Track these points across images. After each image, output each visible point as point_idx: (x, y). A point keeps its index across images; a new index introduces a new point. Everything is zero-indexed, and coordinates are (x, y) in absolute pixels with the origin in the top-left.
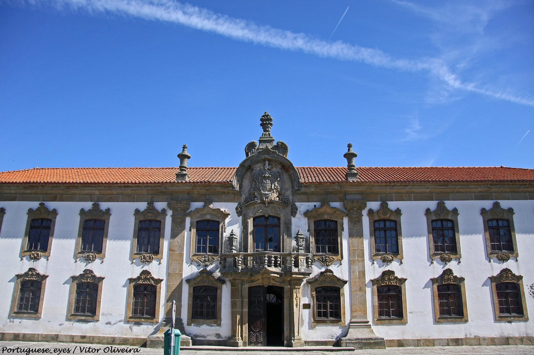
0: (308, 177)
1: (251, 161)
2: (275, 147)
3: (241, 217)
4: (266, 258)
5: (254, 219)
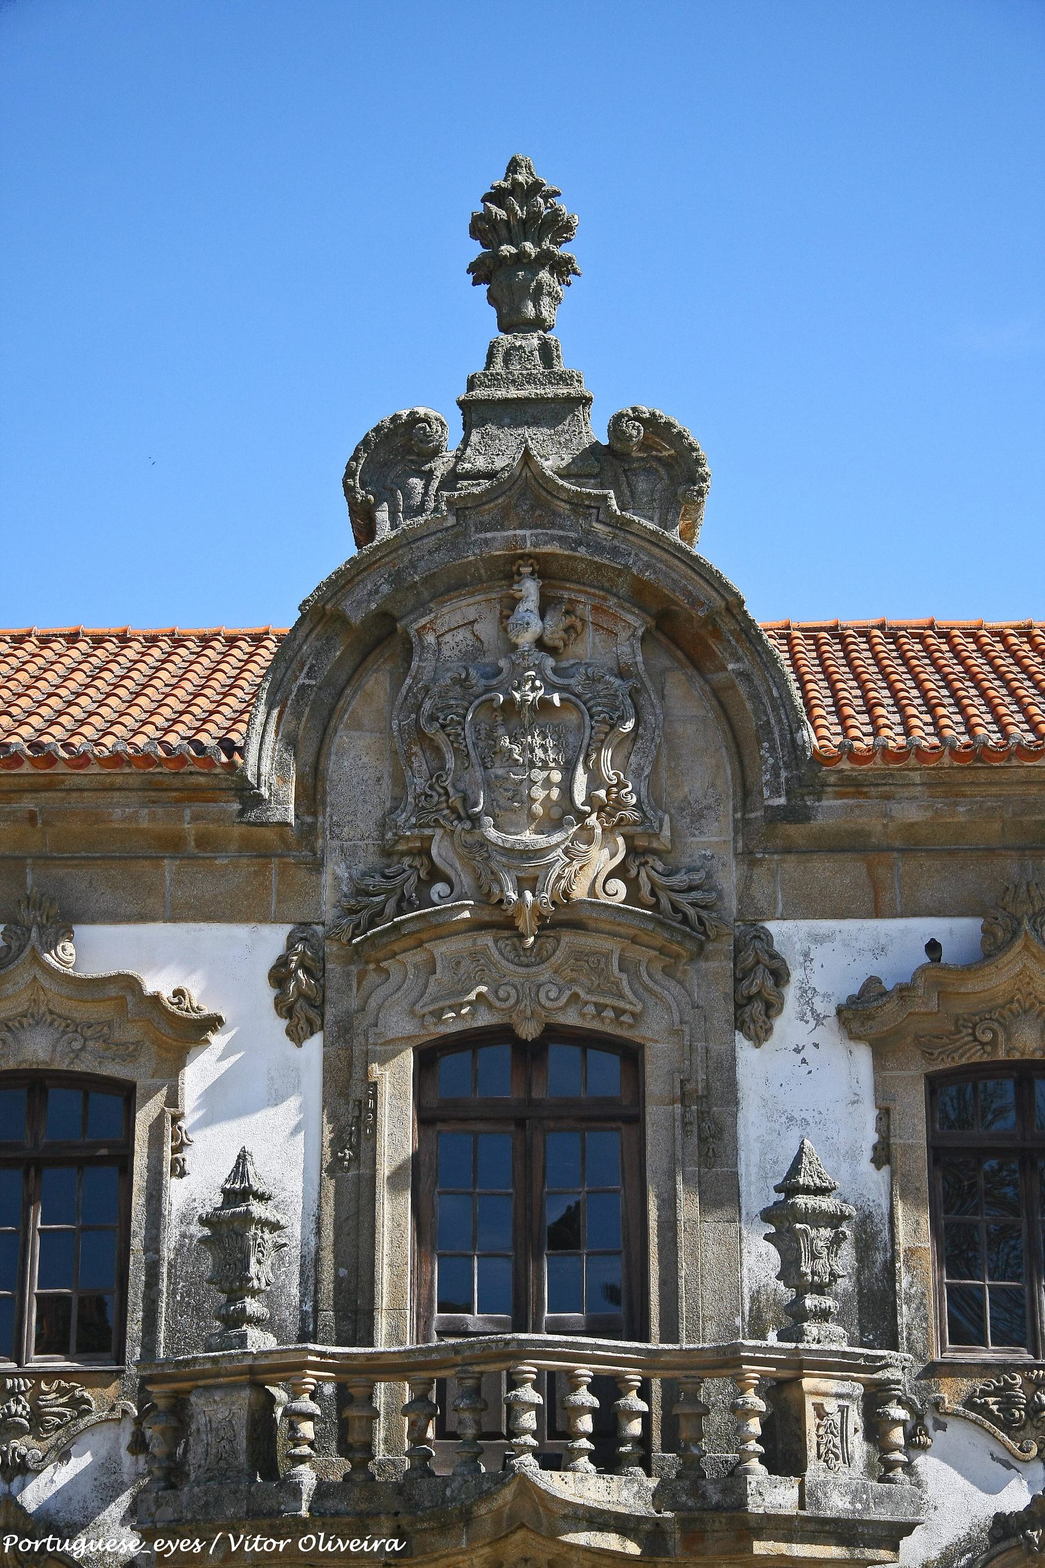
0: (869, 708)
1: (396, 579)
2: (606, 461)
3: (315, 1045)
4: (529, 1394)
5: (427, 1060)
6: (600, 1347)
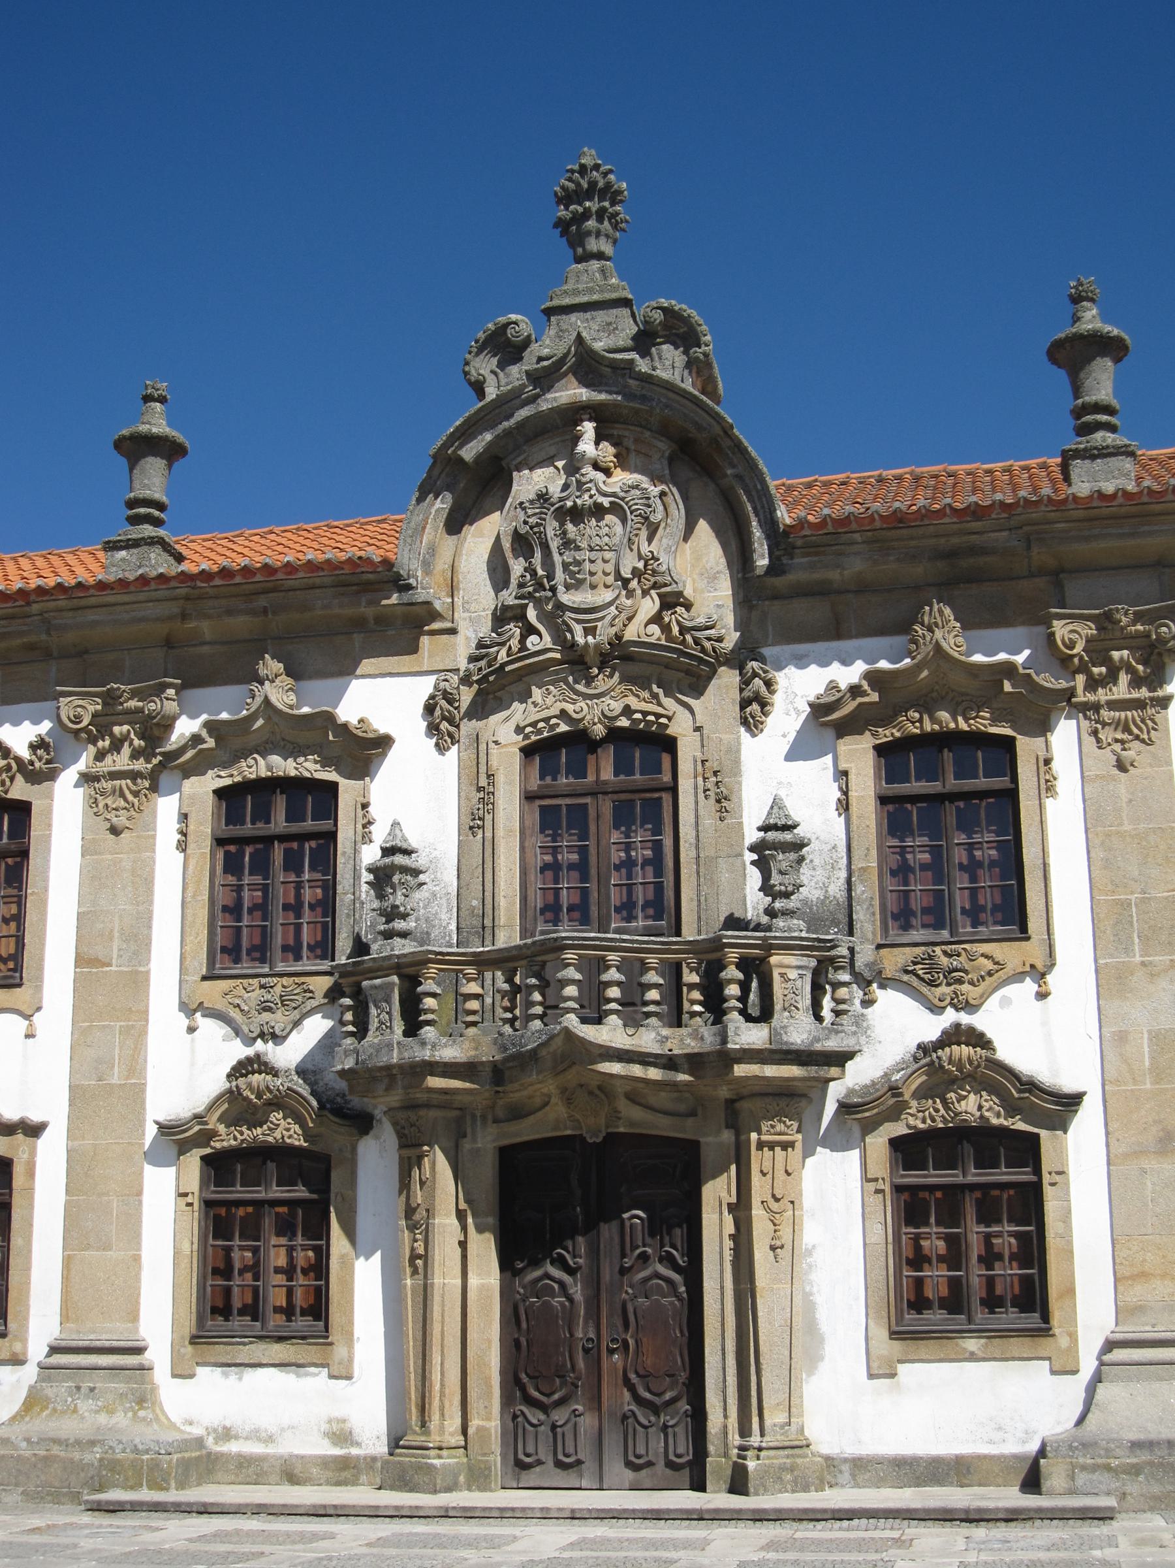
6: (624, 941)
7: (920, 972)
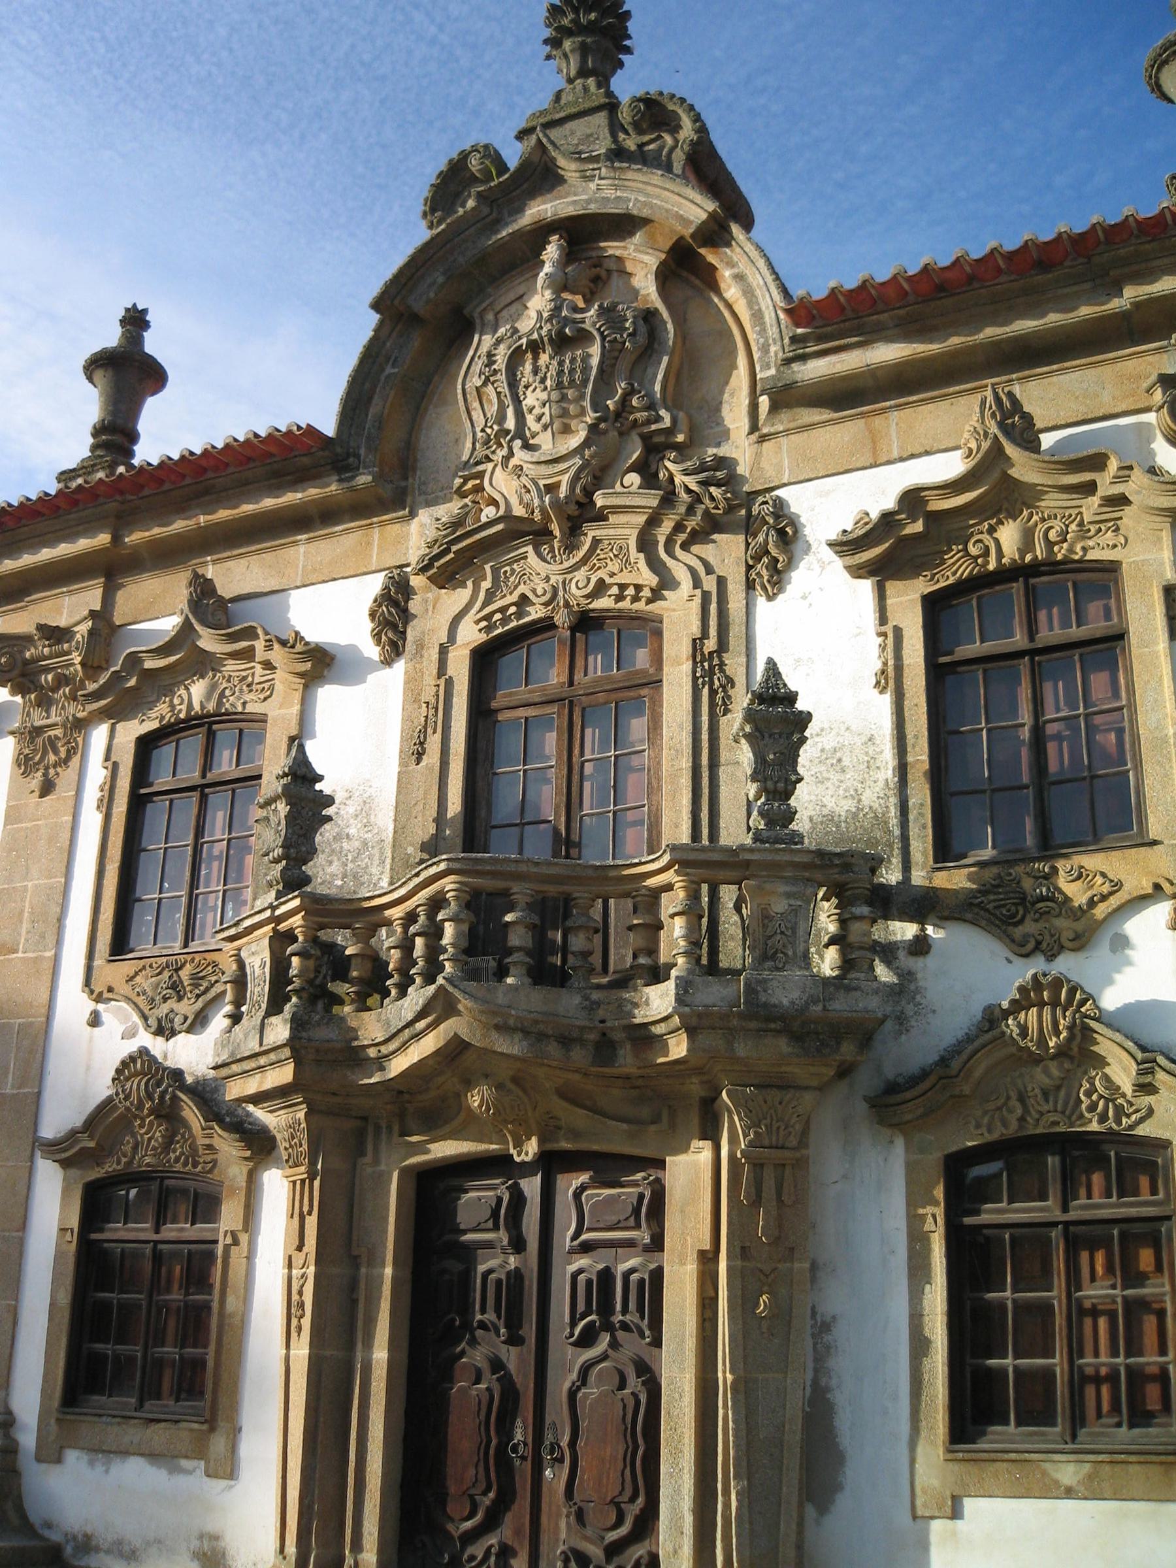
7: (990, 906)
